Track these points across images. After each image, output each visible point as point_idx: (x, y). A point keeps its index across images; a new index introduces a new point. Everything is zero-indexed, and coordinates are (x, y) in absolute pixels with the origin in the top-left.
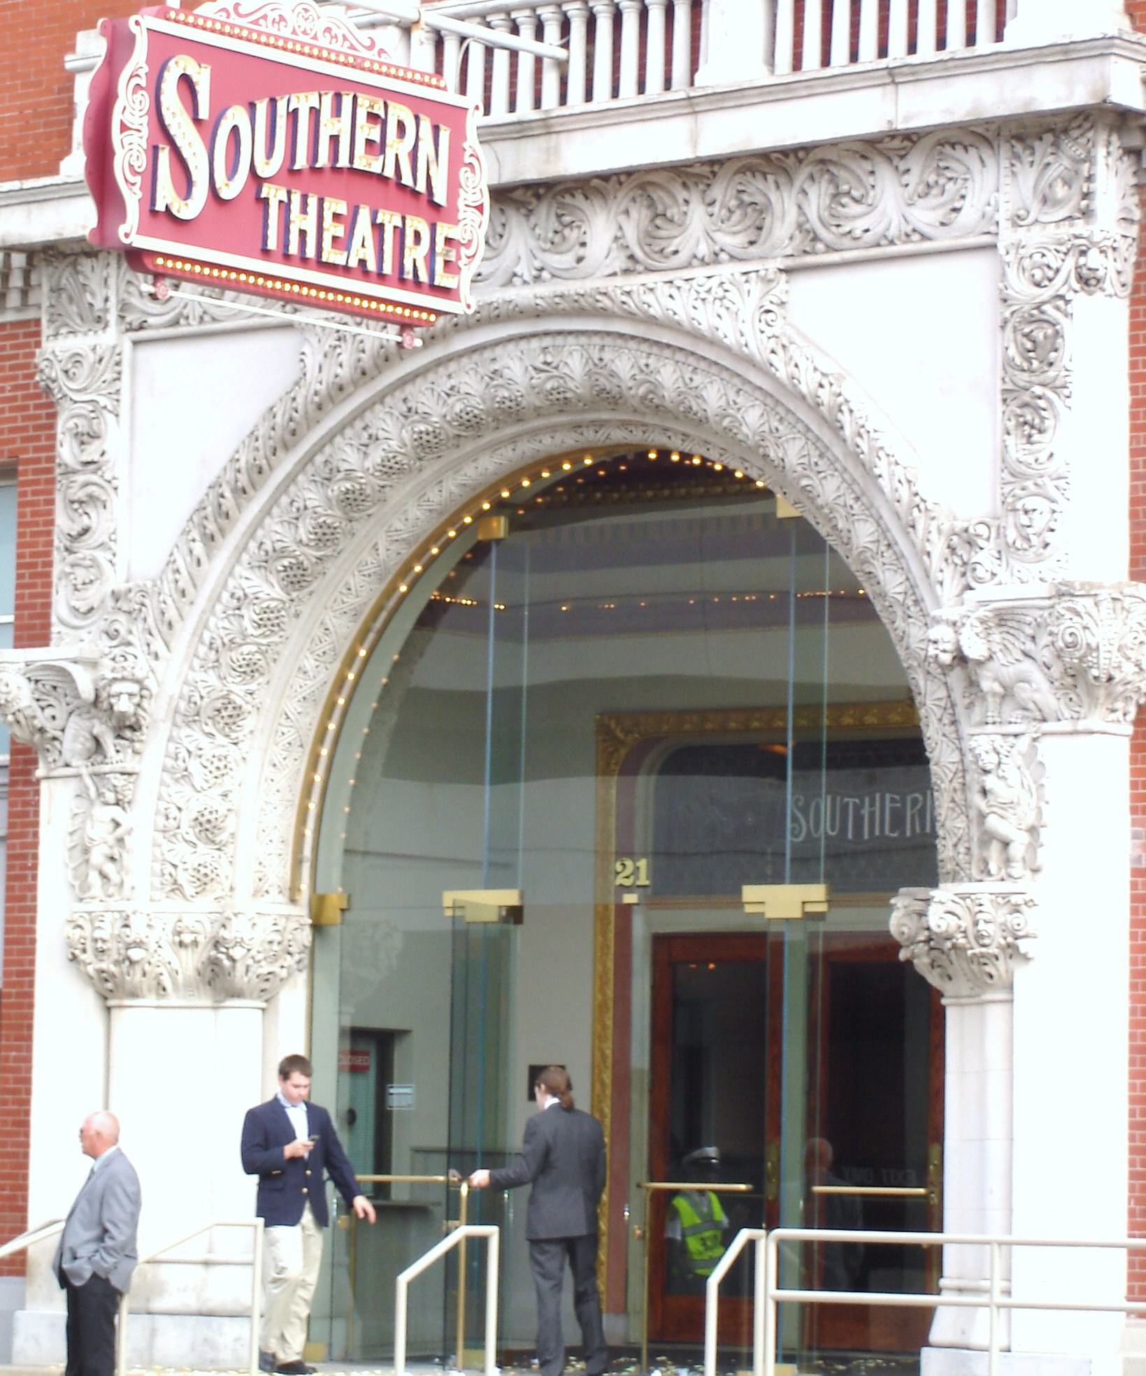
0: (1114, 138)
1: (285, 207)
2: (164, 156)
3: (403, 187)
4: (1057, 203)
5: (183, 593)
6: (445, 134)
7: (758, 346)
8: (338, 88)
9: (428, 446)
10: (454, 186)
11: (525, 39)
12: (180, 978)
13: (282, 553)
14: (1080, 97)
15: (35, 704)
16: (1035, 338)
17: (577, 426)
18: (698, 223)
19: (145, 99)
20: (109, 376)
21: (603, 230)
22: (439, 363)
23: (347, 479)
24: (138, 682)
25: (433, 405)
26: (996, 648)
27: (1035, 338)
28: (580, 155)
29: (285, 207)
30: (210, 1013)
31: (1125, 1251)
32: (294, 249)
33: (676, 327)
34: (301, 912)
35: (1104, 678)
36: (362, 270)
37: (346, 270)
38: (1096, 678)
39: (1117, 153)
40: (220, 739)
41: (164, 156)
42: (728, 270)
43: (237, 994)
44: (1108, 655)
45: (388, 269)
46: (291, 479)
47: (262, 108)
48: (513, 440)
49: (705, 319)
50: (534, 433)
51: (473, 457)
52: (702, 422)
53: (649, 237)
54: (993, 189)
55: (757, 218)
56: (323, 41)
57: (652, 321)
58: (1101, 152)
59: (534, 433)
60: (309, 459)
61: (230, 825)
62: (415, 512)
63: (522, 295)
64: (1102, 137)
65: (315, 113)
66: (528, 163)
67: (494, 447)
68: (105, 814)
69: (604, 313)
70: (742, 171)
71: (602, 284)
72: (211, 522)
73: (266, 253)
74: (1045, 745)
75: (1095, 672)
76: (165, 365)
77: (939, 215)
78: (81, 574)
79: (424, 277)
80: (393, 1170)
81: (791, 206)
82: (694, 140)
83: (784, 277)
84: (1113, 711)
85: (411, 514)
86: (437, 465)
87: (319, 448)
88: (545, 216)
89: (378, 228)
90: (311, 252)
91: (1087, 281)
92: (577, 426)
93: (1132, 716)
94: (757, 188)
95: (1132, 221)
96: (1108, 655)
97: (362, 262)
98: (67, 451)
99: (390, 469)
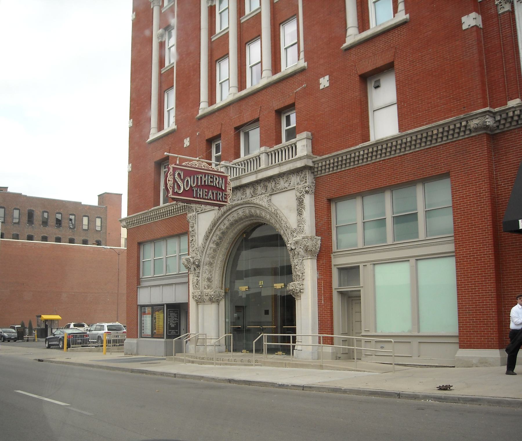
1: (197, 191)
2: (176, 184)
4: (303, 181)
6: (224, 181)
7: (267, 206)
8: (205, 174)
9: (232, 225)
10: (226, 187)
11: (240, 166)
13: (215, 241)
14: (303, 165)
16: (300, 202)
17: (250, 220)
18: (260, 189)
19: (172, 176)
21: (249, 191)
22: (231, 213)
25: (231, 218)
27: (300, 202)
28: (245, 181)
29: (197, 191)
32: (198, 196)
33: (258, 204)
34: (223, 291)
36: (210, 199)
37: (208, 199)
39: (310, 173)
41: (176, 184)
42: (263, 196)
43: (214, 302)
45: (215, 199)
46: (215, 231)
47: (192, 178)
48: (243, 223)
49: (261, 203)
50: (245, 222)
51: (238, 226)
52: (263, 218)
53: (253, 192)
54: (295, 179)
55: (266, 187)
56: (203, 168)
57: (254, 204)
58: (307, 173)
59: (245, 222)
60: (217, 228)
61: (213, 279)
62: (232, 234)
63: (239, 202)
65: (201, 177)
66: (237, 183)
67: (240, 224)
68: (196, 278)
69: (249, 203)
70: (265, 181)
71: (249, 199)
72: (207, 237)
73: (194, 198)
74: (304, 261)
76: (201, 216)
77: (288, 185)
78: (193, 246)
80: (34, 239)
81: (271, 185)
82: (257, 177)
85: (231, 235)
87: (218, 226)
88: (242, 191)
89: (213, 193)
90: (201, 196)
91: (307, 192)
92: (250, 220)
94: (266, 183)
97: (210, 198)
98: (190, 229)
99: (227, 228)
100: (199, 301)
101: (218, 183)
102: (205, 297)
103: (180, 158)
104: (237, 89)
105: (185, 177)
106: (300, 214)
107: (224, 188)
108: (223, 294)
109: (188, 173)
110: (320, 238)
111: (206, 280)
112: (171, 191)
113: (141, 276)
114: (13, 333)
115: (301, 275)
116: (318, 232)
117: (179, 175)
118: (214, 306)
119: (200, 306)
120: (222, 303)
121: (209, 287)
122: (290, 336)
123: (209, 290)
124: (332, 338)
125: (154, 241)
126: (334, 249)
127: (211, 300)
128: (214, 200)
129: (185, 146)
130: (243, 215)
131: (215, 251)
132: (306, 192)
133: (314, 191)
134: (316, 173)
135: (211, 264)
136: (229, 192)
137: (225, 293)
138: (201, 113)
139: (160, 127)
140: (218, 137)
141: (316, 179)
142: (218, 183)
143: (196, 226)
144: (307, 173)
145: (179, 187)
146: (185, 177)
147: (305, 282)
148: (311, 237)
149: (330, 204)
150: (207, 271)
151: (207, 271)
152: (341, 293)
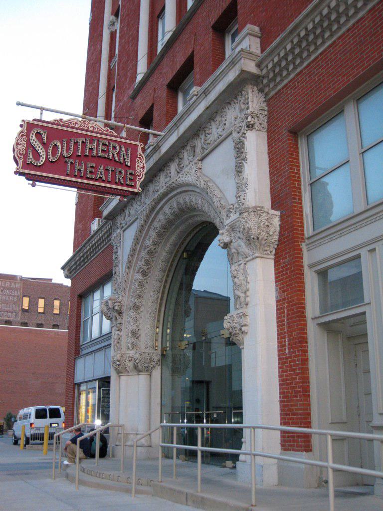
0: (255, 87)
3: (115, 161)
5: (126, 281)
8: (92, 139)
10: (133, 162)
12: (130, 368)
15: (107, 311)
20: (119, 239)
23: (147, 248)
24: (120, 302)
26: (233, 238)
30: (137, 376)
31: (279, 432)
35: (256, 238)
37: (96, 180)
38: (253, 238)
40: (135, 313)
44: (255, 230)
61: (140, 333)
64: (250, 87)
73: (68, 175)
75: (252, 237)
79: (122, 181)
83: (200, 162)
84: (266, 251)
85: (163, 253)
86: (164, 240)
91: (250, 126)
93: (274, 252)
95: (265, 110)
96: (255, 230)
102: (128, 363)
106: (239, 170)
108: (159, 357)
110: (278, 213)
111: (130, 335)
113: (81, 343)
114: (53, 425)
115: (242, 295)
116: (276, 203)
117: (38, 135)
118: (143, 378)
120: (157, 373)
121: (134, 346)
122: (196, 428)
123: (134, 351)
124: (307, 437)
126: (308, 230)
127: (137, 369)
128: (109, 182)
130: (172, 214)
132: (248, 126)
133: (265, 124)
134: (266, 90)
137: (163, 355)
142: (119, 154)
143: (120, 251)
144: (250, 91)
145: (37, 155)
147: (249, 311)
148: (255, 207)
149: (297, 141)
150: (131, 320)
151: (131, 320)
152: (328, 327)
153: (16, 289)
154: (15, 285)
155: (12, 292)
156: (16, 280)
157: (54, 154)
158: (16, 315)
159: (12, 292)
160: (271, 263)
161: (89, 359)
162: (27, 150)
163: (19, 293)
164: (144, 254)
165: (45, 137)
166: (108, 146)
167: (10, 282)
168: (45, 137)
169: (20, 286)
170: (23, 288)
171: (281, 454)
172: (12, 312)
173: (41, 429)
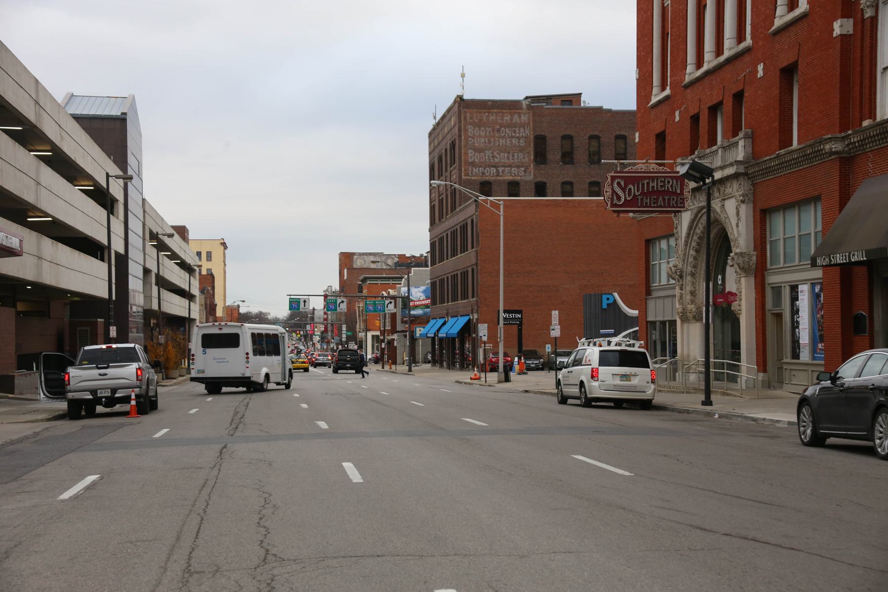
8: (653, 178)
10: (682, 189)
36: (661, 206)
89: (664, 200)
100: (685, 319)
101: (672, 186)
103: (621, 164)
104: (694, 66)
105: (626, 185)
107: (679, 192)
109: (629, 180)
112: (609, 204)
117: (618, 184)
119: (685, 325)
125: (786, 207)
126: (768, 266)
129: (835, 35)
131: (695, 258)
135: (693, 275)
136: (687, 194)
138: (687, 79)
139: (699, 63)
140: (720, 103)
141: (754, 185)
143: (679, 227)
145: (619, 198)
146: (626, 185)
153: (523, 125)
154: (520, 117)
155: (515, 132)
156: (521, 108)
157: (629, 195)
158: (525, 171)
159: (515, 132)
160: (753, 278)
161: (660, 302)
162: (612, 195)
163: (527, 131)
164: (692, 252)
165: (622, 184)
166: (664, 182)
167: (510, 113)
168: (622, 184)
169: (529, 119)
170: (534, 121)
171: (195, 303)
172: (518, 167)
173: (238, 410)
